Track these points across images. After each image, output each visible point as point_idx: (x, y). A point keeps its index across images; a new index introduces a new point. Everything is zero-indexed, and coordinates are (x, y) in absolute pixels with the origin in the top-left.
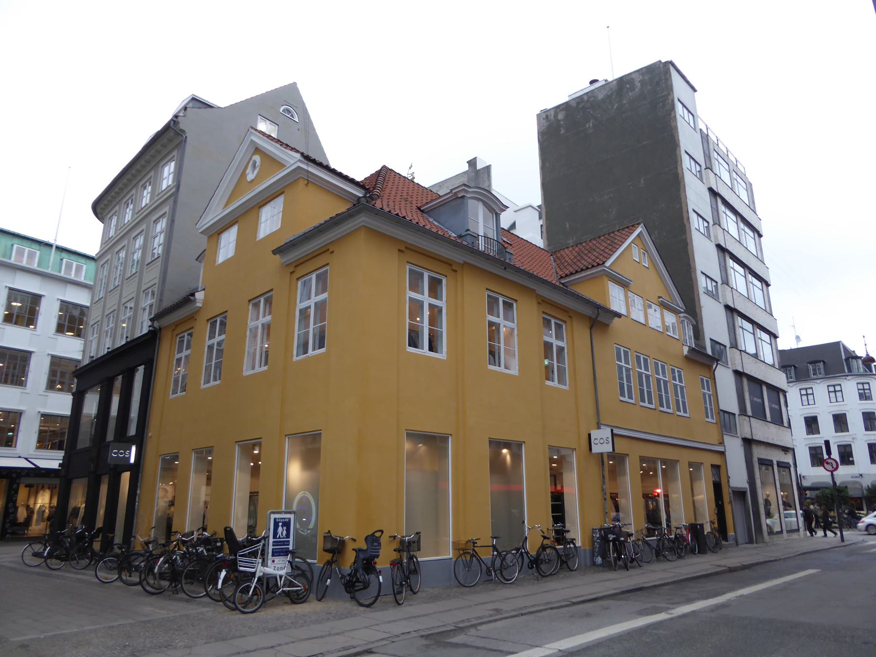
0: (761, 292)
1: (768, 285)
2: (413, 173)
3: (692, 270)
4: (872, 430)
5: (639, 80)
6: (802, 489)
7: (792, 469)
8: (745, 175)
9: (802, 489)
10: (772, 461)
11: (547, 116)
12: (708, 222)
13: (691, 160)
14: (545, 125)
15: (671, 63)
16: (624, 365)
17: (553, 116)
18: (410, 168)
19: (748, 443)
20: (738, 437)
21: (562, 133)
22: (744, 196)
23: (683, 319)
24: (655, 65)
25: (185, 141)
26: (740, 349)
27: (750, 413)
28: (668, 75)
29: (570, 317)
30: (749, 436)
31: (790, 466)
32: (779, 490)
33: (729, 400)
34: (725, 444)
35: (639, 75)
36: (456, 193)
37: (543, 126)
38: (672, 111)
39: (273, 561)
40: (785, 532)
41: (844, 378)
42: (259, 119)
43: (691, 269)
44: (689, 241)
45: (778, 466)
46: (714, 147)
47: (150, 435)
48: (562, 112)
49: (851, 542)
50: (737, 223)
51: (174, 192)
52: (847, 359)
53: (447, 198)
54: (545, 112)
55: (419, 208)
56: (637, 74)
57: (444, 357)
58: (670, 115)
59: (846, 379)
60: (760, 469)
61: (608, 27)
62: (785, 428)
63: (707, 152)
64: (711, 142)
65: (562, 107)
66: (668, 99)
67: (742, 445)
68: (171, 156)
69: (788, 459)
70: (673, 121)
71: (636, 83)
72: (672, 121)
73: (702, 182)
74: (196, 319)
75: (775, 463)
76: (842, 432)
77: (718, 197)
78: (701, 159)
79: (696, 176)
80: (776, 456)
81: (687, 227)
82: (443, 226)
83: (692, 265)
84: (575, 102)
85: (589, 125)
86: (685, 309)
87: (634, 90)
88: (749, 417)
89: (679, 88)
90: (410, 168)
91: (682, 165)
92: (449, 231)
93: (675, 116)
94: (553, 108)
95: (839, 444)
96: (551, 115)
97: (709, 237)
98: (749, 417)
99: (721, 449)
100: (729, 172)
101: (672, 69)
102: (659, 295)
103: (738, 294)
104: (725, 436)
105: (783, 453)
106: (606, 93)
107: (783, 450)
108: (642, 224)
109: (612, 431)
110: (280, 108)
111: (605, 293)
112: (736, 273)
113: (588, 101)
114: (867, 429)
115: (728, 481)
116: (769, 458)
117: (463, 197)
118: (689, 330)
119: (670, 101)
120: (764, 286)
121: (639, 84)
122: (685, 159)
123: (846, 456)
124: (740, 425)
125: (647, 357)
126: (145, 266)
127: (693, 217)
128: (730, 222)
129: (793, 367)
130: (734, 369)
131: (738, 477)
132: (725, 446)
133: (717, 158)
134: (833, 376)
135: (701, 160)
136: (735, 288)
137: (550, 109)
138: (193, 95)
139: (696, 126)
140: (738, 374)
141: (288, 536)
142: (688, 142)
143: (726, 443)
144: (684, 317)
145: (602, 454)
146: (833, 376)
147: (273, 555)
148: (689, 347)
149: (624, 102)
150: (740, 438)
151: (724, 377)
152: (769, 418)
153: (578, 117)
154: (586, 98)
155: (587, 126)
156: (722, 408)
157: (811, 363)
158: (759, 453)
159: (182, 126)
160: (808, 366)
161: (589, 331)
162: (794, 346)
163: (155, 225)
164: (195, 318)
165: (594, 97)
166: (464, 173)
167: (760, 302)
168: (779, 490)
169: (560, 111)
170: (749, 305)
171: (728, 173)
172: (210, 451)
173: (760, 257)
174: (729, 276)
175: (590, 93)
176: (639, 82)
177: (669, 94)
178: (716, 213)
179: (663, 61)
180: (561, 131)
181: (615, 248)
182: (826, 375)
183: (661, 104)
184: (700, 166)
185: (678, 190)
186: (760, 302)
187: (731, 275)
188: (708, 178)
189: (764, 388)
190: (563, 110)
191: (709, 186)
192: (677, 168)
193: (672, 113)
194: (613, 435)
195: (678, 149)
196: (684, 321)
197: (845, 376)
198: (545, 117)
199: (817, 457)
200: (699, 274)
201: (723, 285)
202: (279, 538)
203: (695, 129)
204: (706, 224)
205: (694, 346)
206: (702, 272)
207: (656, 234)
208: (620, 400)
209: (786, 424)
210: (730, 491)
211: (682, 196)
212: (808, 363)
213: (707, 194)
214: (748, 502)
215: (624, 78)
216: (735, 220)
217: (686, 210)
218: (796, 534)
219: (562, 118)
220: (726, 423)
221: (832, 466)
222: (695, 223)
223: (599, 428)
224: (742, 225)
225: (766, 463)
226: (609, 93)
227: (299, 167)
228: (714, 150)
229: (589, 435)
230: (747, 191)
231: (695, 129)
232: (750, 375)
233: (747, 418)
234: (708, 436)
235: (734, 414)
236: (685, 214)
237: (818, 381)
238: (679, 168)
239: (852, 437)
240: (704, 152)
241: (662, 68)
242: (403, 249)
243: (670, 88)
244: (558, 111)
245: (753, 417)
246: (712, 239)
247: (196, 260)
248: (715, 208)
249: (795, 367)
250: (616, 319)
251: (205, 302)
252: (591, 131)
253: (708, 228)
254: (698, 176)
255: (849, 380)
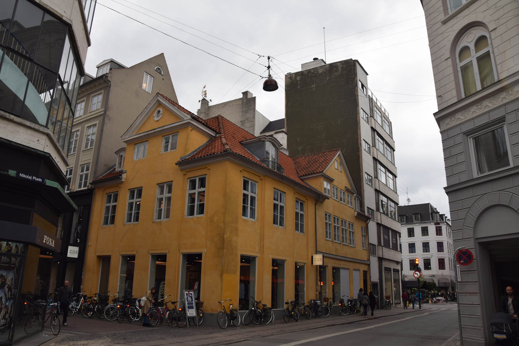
0: (392, 181)
1: (396, 177)
2: (206, 91)
3: (361, 171)
4: (441, 252)
5: (340, 67)
6: (403, 282)
7: (400, 273)
8: (389, 118)
9: (403, 282)
10: (391, 269)
11: (291, 77)
12: (370, 145)
13: (364, 112)
14: (289, 82)
15: (357, 61)
16: (328, 222)
17: (294, 77)
18: (204, 88)
19: (381, 260)
20: (376, 257)
21: (298, 88)
22: (387, 129)
23: (355, 197)
24: (349, 61)
25: (110, 87)
26: (380, 212)
27: (382, 245)
28: (355, 68)
29: (307, 199)
30: (381, 256)
31: (399, 271)
32: (393, 283)
33: (373, 239)
34: (370, 261)
35: (341, 64)
36: (260, 139)
37: (289, 82)
38: (356, 86)
39: (189, 311)
40: (394, 304)
41: (429, 223)
42: (145, 74)
43: (360, 170)
44: (360, 156)
45: (393, 271)
46: (375, 104)
47: (90, 244)
48: (299, 76)
49: (424, 309)
50: (383, 145)
51: (103, 114)
52: (432, 213)
53: (255, 140)
54: (289, 74)
55: (240, 142)
56: (340, 63)
57: (255, 220)
58: (355, 88)
59: (430, 224)
60: (385, 272)
61: (324, 28)
62: (399, 252)
63: (371, 108)
64: (373, 102)
65: (299, 73)
66: (354, 79)
67: (377, 261)
68: (100, 92)
69: (399, 267)
70: (357, 92)
71: (339, 68)
72: (356, 91)
73: (368, 124)
74: (120, 188)
75: (392, 269)
76: (426, 252)
77: (375, 132)
78: (368, 112)
79: (366, 121)
80: (393, 266)
81: (360, 148)
82: (252, 153)
83: (361, 169)
84: (306, 72)
85: (314, 86)
86: (357, 192)
87: (338, 71)
88: (382, 246)
89: (359, 72)
90: (204, 88)
91: (359, 116)
92: (255, 156)
93: (357, 90)
94: (294, 73)
95: (424, 258)
96: (293, 77)
97: (370, 153)
98: (382, 246)
99: (368, 263)
100: (381, 117)
101: (357, 63)
102: (346, 186)
103: (381, 183)
104: (370, 257)
105: (396, 264)
106: (323, 70)
107: (396, 263)
108: (340, 150)
109: (323, 255)
110: (155, 67)
111: (321, 185)
112: (381, 171)
113: (313, 73)
114: (438, 251)
115: (370, 279)
116: (390, 267)
117: (264, 141)
118: (358, 204)
119: (356, 81)
120: (392, 151)
121: (340, 69)
122: (361, 112)
123: (427, 264)
124: (377, 251)
125: (338, 218)
126: (81, 151)
127: (363, 143)
128: (380, 144)
129: (405, 216)
130: (377, 222)
131: (375, 277)
132: (370, 261)
133: (376, 110)
134: (424, 222)
135: (368, 113)
136: (380, 180)
137: (293, 74)
138: (112, 59)
139: (367, 94)
140: (379, 225)
141: (192, 301)
142: (363, 103)
143: (371, 260)
144: (356, 196)
145: (317, 266)
146: (424, 222)
147: (188, 309)
148: (357, 212)
149: (332, 77)
150: (377, 257)
151: (372, 226)
152: (391, 247)
153: (308, 80)
154: (312, 71)
155: (312, 86)
156: (370, 242)
157: (414, 214)
158: (385, 264)
159: (109, 79)
160: (412, 216)
161: (314, 206)
162: (407, 205)
163: (87, 129)
164: (120, 187)
165: (317, 71)
166: (240, 99)
167: (392, 187)
168: (393, 283)
169: (298, 75)
170: (387, 188)
171: (381, 118)
172: (133, 258)
173: (391, 136)
174: (378, 174)
175: (315, 69)
176: (340, 68)
177: (355, 77)
178: (374, 140)
179: (353, 59)
180: (298, 86)
181: (328, 163)
182: (421, 221)
183: (351, 82)
184: (368, 115)
185: (357, 128)
186: (392, 187)
187: (379, 173)
188: (371, 122)
189: (390, 232)
190: (300, 75)
191: (371, 126)
192: (356, 117)
193: (356, 87)
194: (323, 257)
195: (358, 108)
196: (356, 198)
197: (430, 222)
198: (289, 77)
199: (414, 266)
200: (364, 173)
201: (375, 179)
202: (189, 301)
203: (366, 96)
204: (369, 146)
205: (359, 211)
206: (366, 172)
207: (344, 150)
208: (326, 240)
209: (399, 250)
210: (371, 284)
211: (359, 132)
212: (413, 214)
213: (370, 129)
214: (378, 289)
215: (333, 64)
216: (382, 143)
217: (360, 140)
218: (399, 305)
219: (299, 80)
220: (371, 249)
221: (418, 275)
222: (364, 146)
223: (316, 253)
224: (385, 145)
225: (388, 270)
226: (325, 71)
227: (189, 122)
228: (375, 106)
229: (312, 257)
230: (389, 127)
231: (366, 96)
232: (384, 225)
233: (381, 247)
234: (363, 255)
235: (375, 245)
236: (359, 142)
237: (417, 224)
238: (358, 117)
239: (431, 255)
240: (370, 108)
241: (352, 63)
242: (242, 170)
243: (355, 74)
244: (297, 75)
245: (384, 247)
246: (371, 154)
247: (115, 153)
248: (374, 138)
249: (406, 216)
250: (327, 200)
251: (126, 179)
252: (314, 89)
253: (369, 148)
254: (367, 121)
255: (432, 224)
